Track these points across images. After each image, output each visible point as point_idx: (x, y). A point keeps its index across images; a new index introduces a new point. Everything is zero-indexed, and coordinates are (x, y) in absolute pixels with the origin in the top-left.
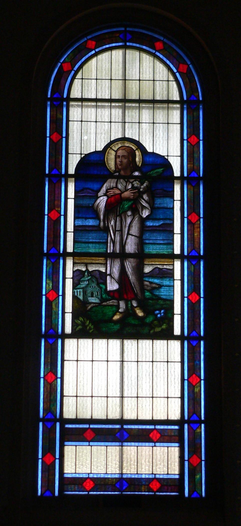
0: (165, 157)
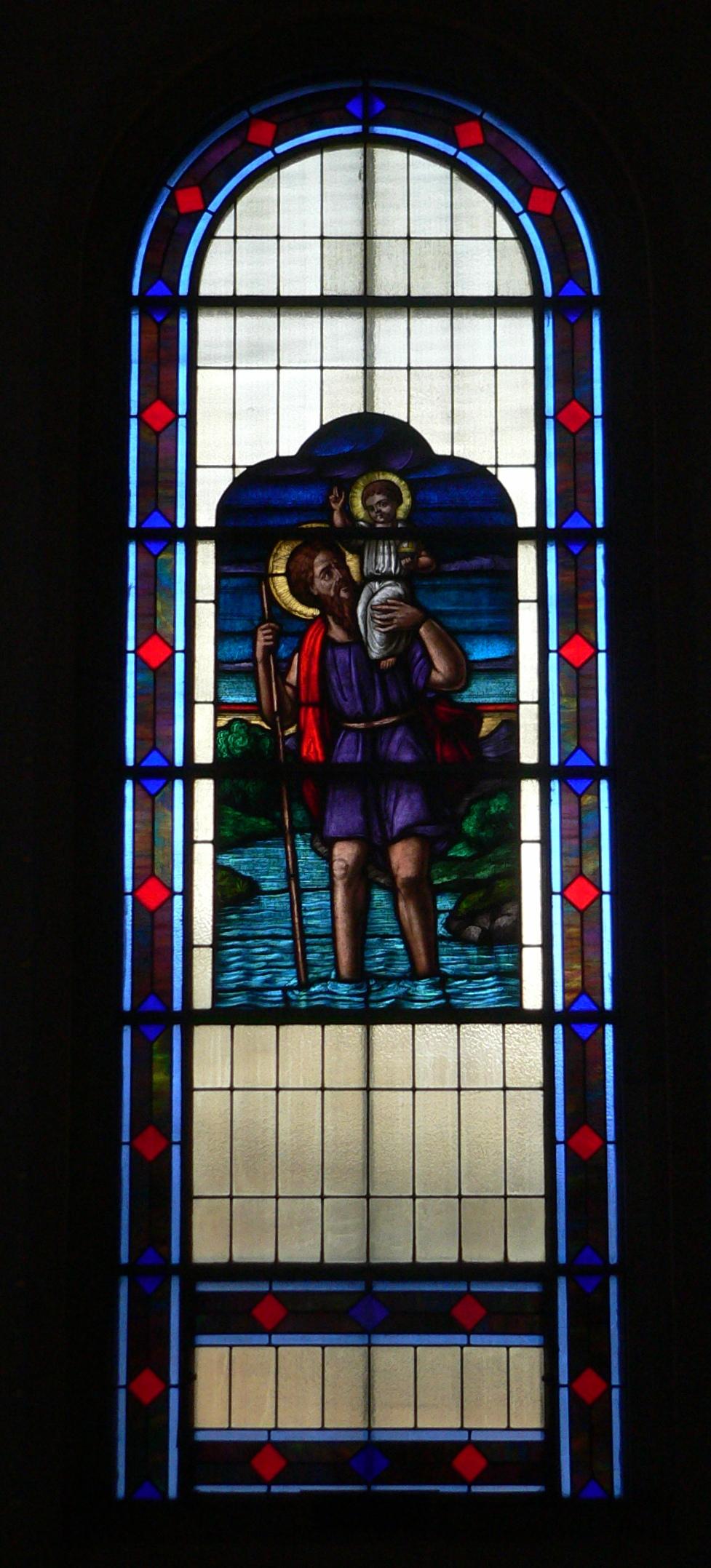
0: (489, 469)
